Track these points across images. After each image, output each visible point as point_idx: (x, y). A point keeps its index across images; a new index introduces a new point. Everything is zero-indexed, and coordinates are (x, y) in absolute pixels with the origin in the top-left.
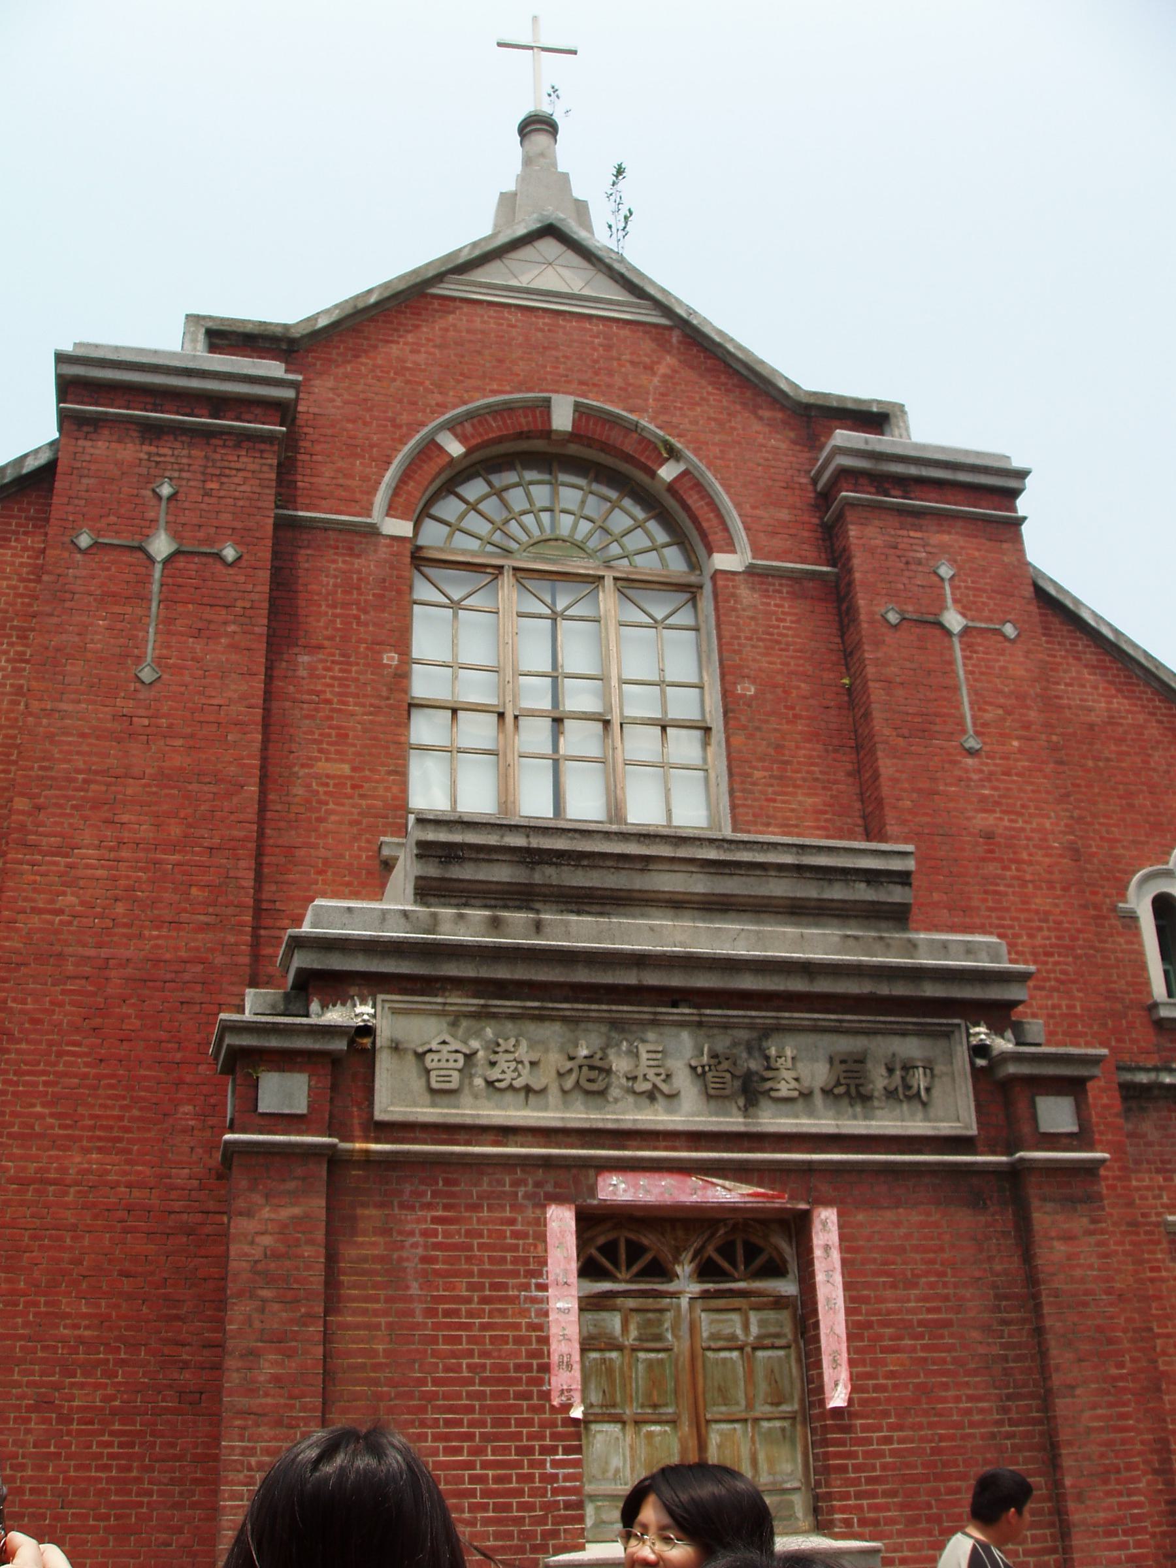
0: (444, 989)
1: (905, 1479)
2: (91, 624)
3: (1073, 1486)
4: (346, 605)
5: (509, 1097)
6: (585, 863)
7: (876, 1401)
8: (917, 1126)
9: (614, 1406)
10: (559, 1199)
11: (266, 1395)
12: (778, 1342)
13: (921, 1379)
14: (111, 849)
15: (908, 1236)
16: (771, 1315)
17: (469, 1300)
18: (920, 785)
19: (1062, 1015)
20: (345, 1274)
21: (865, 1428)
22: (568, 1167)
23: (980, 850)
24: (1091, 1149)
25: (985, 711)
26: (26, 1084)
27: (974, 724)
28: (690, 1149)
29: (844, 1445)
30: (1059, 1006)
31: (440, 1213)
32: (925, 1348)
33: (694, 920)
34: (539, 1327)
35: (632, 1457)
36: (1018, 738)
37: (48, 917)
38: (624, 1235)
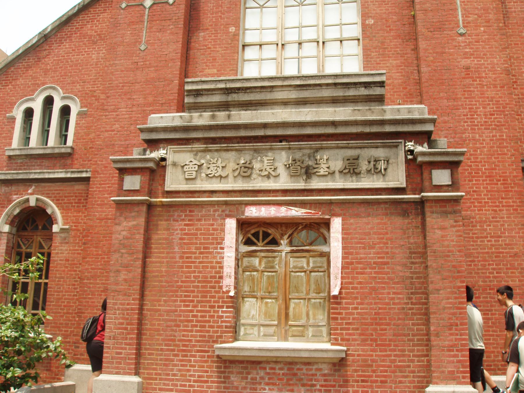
0: (193, 142)
1: (362, 324)
2: (126, 33)
3: (434, 330)
4: (217, 13)
5: (214, 180)
6: (248, 91)
7: (353, 293)
8: (380, 184)
9: (254, 292)
10: (230, 216)
11: (122, 285)
12: (320, 270)
13: (373, 285)
14: (130, 108)
15: (372, 228)
16: (319, 259)
17: (195, 253)
18: (437, 51)
19: (497, 139)
20: (153, 244)
21: (347, 303)
22: (234, 204)
23: (463, 75)
24: (458, 191)
25: (469, 17)
26: (102, 188)
27: (463, 23)
28: (283, 196)
29: (338, 310)
30: (496, 136)
31: (187, 222)
32: (376, 273)
33: (292, 108)
34: (220, 263)
35: (259, 311)
36: (483, 26)
37: (110, 133)
38: (261, 230)
